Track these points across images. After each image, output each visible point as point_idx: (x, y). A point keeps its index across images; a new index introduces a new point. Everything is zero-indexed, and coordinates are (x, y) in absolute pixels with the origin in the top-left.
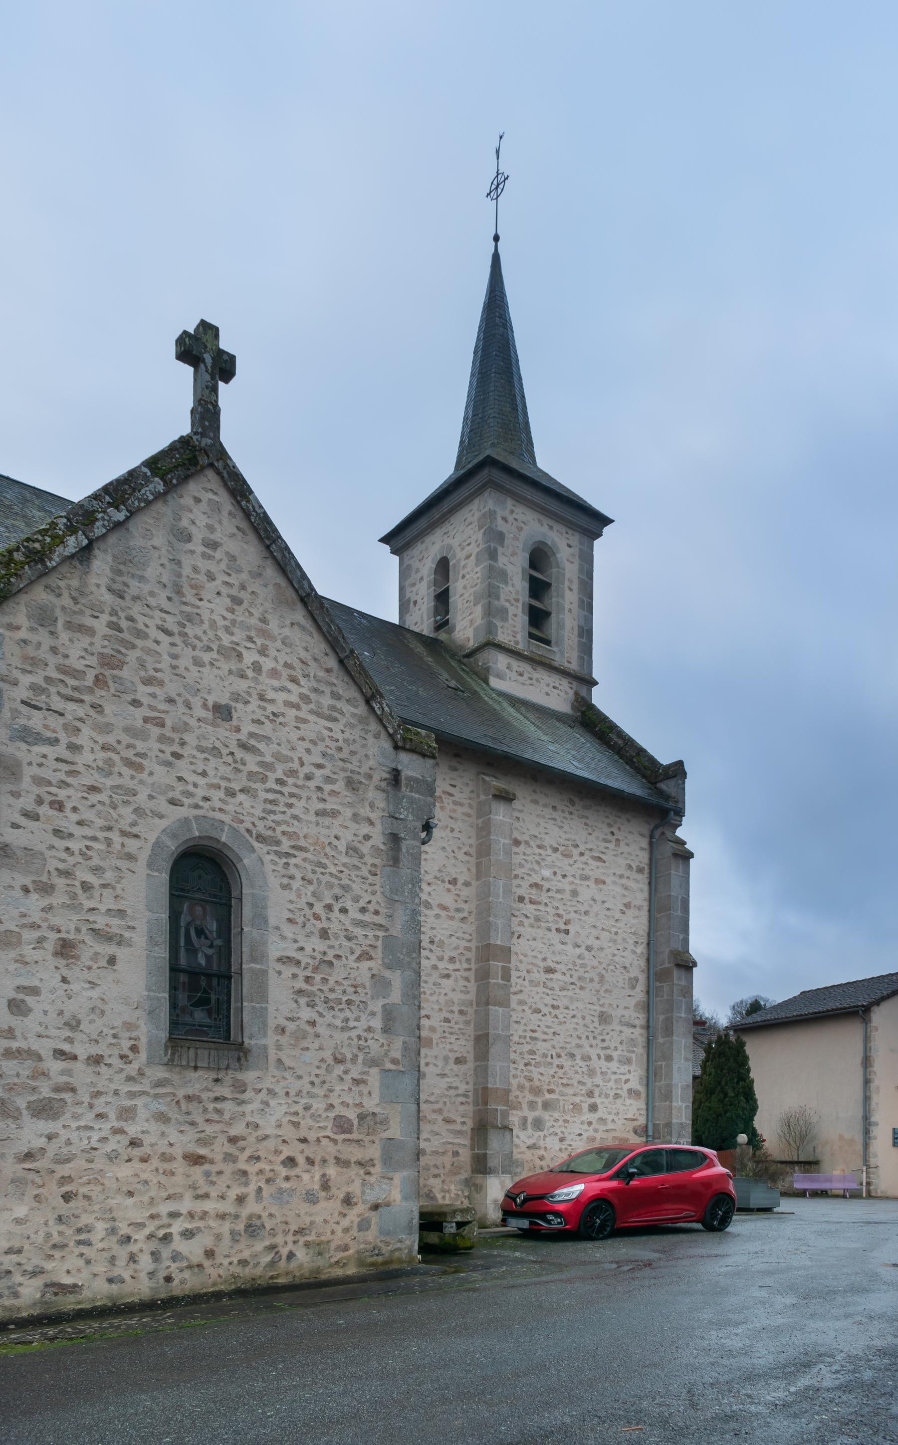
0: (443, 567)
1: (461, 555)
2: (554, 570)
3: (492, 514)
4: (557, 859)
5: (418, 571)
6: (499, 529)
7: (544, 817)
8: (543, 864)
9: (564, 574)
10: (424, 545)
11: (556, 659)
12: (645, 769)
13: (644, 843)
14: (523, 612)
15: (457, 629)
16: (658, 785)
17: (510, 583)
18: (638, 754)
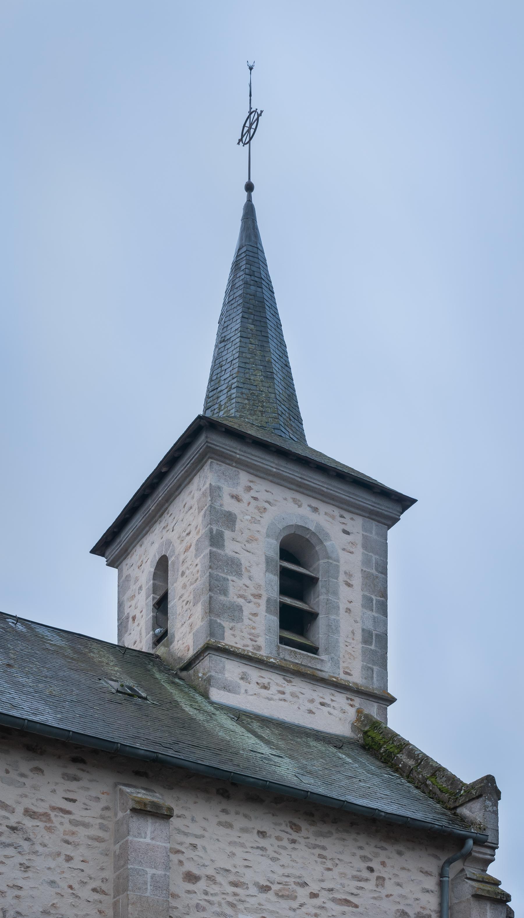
0: (162, 566)
1: (179, 548)
2: (321, 562)
3: (214, 492)
4: (268, 900)
5: (137, 580)
6: (226, 508)
7: (242, 845)
8: (241, 906)
9: (338, 566)
10: (143, 547)
11: (326, 669)
12: (442, 791)
13: (431, 883)
14: (268, 610)
15: (176, 640)
16: (459, 811)
17: (245, 574)
18: (433, 775)
